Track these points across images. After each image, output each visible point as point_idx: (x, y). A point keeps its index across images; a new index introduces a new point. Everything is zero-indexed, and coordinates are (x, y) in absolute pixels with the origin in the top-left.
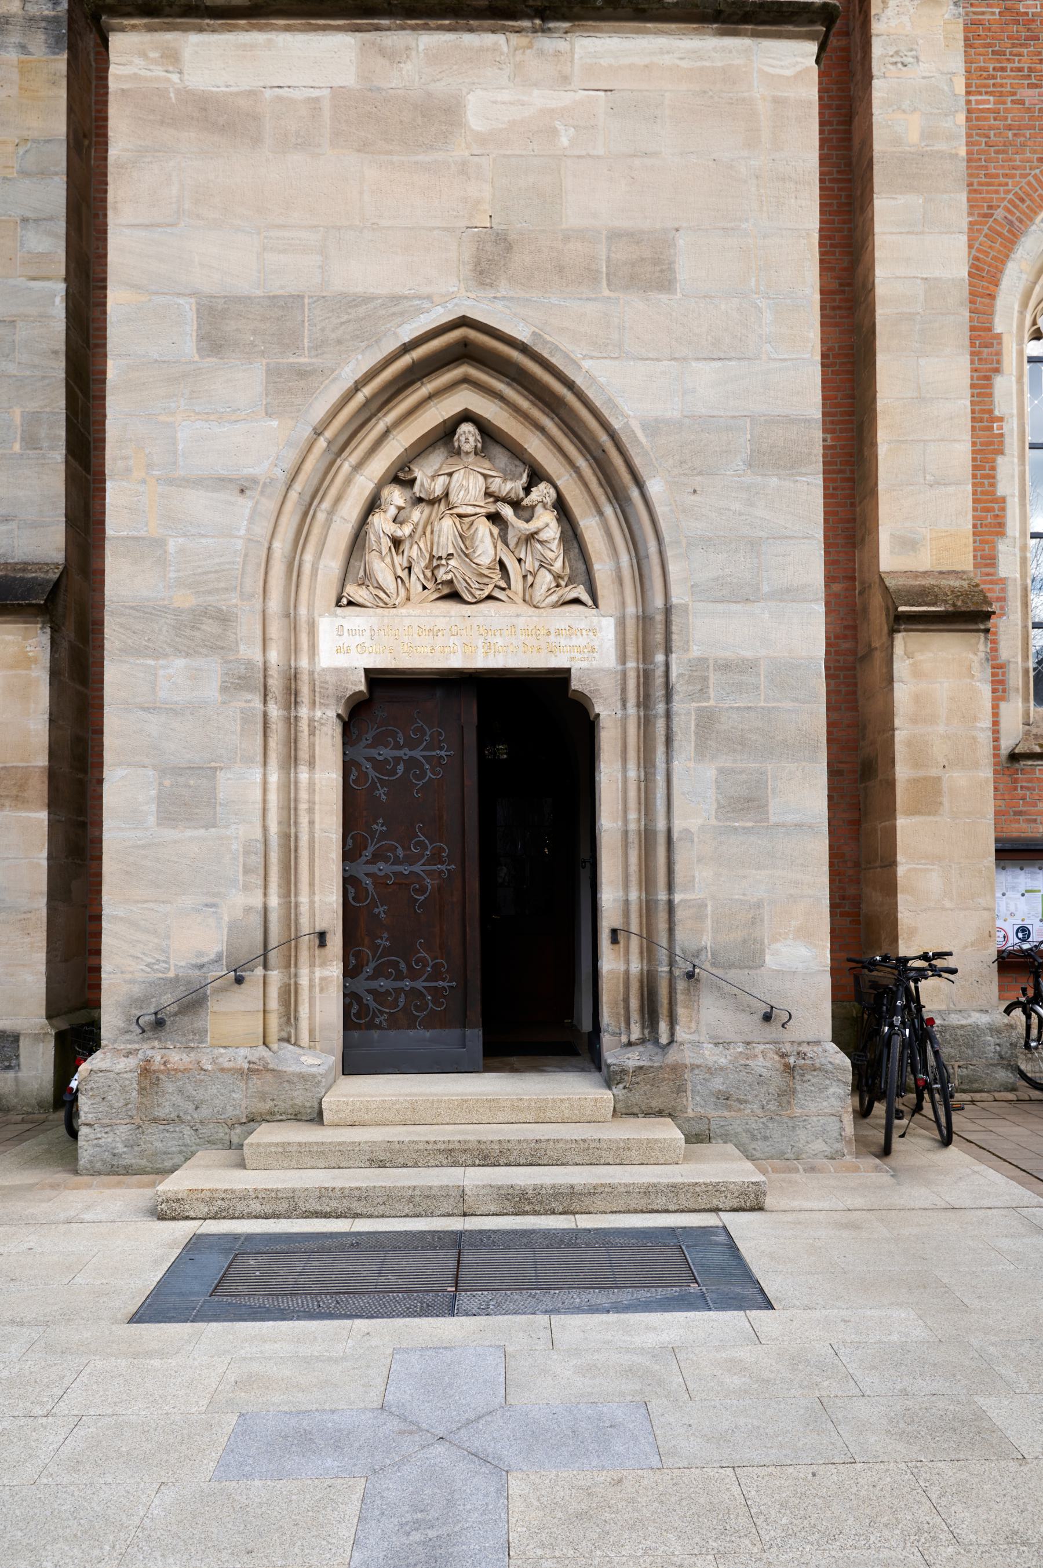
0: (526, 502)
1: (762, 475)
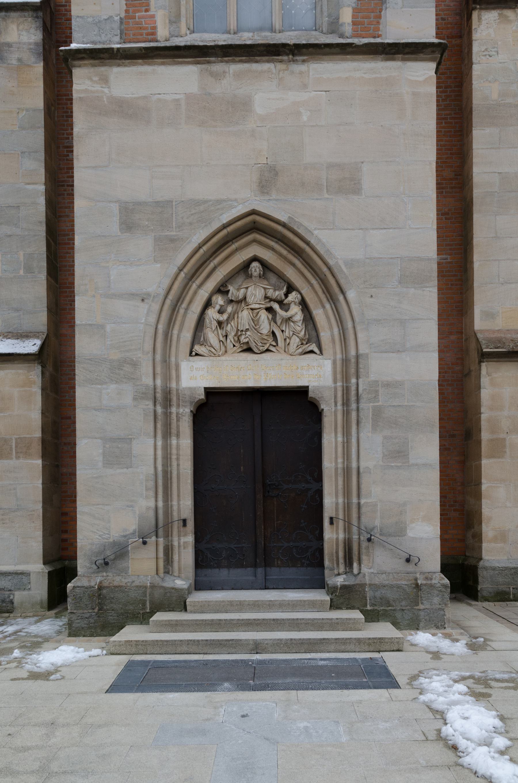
0: (286, 301)
1: (406, 288)
